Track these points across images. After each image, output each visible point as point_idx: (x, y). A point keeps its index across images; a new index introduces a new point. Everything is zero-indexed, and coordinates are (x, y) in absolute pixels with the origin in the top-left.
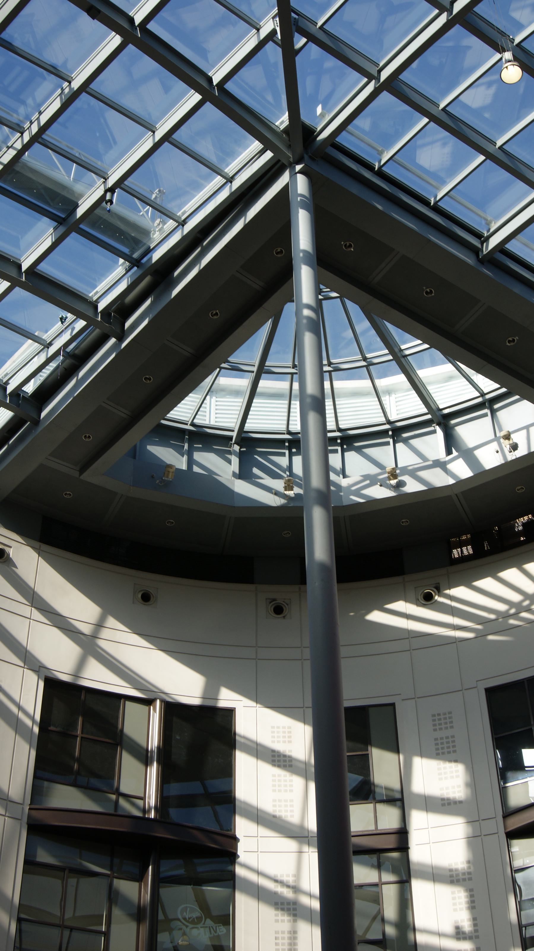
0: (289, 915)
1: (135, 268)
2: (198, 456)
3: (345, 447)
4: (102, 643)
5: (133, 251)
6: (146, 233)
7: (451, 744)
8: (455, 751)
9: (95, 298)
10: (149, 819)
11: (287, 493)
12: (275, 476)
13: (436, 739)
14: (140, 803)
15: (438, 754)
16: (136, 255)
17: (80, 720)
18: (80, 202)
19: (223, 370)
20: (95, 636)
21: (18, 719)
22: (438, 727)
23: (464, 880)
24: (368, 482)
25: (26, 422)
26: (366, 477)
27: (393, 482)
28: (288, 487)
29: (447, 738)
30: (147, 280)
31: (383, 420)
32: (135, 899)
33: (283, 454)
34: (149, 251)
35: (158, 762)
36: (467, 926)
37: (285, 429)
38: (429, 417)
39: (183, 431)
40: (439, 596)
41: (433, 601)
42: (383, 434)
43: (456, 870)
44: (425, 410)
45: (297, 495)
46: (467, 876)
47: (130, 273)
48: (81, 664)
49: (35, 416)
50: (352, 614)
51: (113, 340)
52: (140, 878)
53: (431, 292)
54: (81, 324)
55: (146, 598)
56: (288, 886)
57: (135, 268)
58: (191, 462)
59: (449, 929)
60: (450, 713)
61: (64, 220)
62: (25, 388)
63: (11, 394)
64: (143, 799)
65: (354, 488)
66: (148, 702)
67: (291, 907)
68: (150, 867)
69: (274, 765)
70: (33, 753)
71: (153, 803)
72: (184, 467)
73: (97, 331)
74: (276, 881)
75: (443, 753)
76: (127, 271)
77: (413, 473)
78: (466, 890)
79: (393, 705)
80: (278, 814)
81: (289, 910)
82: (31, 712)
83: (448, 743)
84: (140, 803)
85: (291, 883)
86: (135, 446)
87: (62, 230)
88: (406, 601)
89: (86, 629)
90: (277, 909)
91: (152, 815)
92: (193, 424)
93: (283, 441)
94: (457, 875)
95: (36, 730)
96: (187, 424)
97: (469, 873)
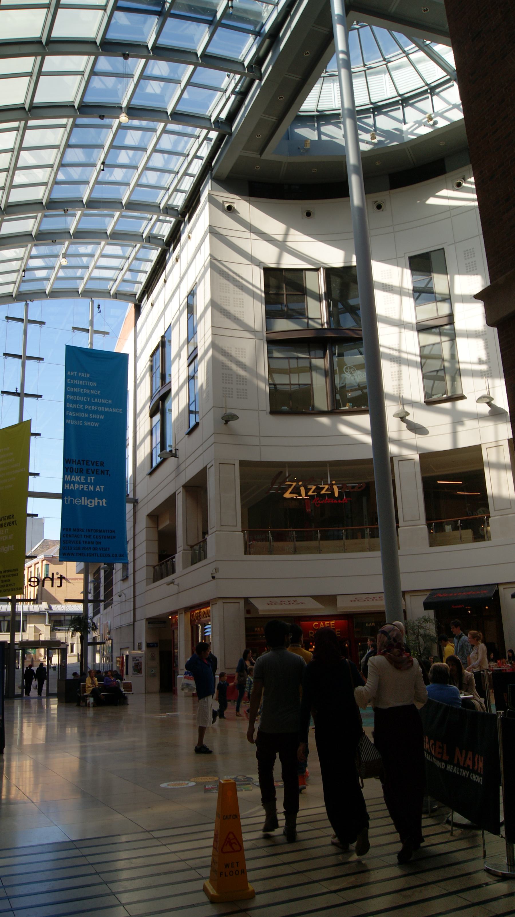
0: (397, 363)
1: (258, 37)
2: (323, 129)
3: (404, 105)
4: (288, 244)
5: (255, 27)
6: (259, 14)
7: (474, 266)
8: (476, 269)
9: (242, 59)
10: (325, 329)
11: (373, 141)
12: (367, 131)
13: (466, 264)
14: (319, 321)
15: (467, 272)
16: (257, 29)
17: (284, 285)
18: (217, 9)
19: (325, 78)
20: (285, 241)
21: (253, 291)
22: (467, 257)
23: (483, 335)
24: (417, 125)
25: (225, 136)
26: (416, 122)
27: (431, 123)
28: (373, 138)
29: (472, 262)
30: (267, 41)
31: (423, 84)
32: (323, 367)
33: (370, 117)
34: (263, 25)
35: (326, 300)
36: (484, 357)
37: (369, 102)
38: (448, 77)
39: (313, 116)
40: (465, 183)
41: (462, 187)
42: (425, 92)
43: (479, 331)
44: (445, 74)
45: (379, 141)
46: (484, 333)
47: (257, 40)
48: (280, 257)
49: (229, 131)
50: (418, 202)
51: (257, 81)
52: (324, 357)
53: (427, 10)
54: (238, 77)
55: (309, 214)
56: (396, 350)
57: (258, 37)
58: (320, 134)
59: (476, 360)
60: (473, 249)
61: (212, 21)
62: (220, 116)
63: (214, 122)
64: (320, 319)
65: (410, 131)
66: (317, 270)
67: (398, 359)
68: (328, 351)
69: (384, 291)
70: (264, 307)
71: (325, 320)
72: (316, 138)
73: (248, 79)
74: (390, 348)
75: (470, 271)
76: (255, 40)
77: (441, 115)
78: (484, 340)
79: (443, 249)
80: (388, 315)
81: (397, 361)
82: (259, 287)
83: (472, 265)
84: (319, 321)
85: (397, 348)
86: (288, 130)
87: (212, 28)
88: (447, 189)
89: (280, 238)
90: (391, 361)
91: (326, 326)
92: (318, 111)
93: (369, 109)
94: (479, 333)
95: (263, 295)
96: (314, 112)
97: (485, 331)
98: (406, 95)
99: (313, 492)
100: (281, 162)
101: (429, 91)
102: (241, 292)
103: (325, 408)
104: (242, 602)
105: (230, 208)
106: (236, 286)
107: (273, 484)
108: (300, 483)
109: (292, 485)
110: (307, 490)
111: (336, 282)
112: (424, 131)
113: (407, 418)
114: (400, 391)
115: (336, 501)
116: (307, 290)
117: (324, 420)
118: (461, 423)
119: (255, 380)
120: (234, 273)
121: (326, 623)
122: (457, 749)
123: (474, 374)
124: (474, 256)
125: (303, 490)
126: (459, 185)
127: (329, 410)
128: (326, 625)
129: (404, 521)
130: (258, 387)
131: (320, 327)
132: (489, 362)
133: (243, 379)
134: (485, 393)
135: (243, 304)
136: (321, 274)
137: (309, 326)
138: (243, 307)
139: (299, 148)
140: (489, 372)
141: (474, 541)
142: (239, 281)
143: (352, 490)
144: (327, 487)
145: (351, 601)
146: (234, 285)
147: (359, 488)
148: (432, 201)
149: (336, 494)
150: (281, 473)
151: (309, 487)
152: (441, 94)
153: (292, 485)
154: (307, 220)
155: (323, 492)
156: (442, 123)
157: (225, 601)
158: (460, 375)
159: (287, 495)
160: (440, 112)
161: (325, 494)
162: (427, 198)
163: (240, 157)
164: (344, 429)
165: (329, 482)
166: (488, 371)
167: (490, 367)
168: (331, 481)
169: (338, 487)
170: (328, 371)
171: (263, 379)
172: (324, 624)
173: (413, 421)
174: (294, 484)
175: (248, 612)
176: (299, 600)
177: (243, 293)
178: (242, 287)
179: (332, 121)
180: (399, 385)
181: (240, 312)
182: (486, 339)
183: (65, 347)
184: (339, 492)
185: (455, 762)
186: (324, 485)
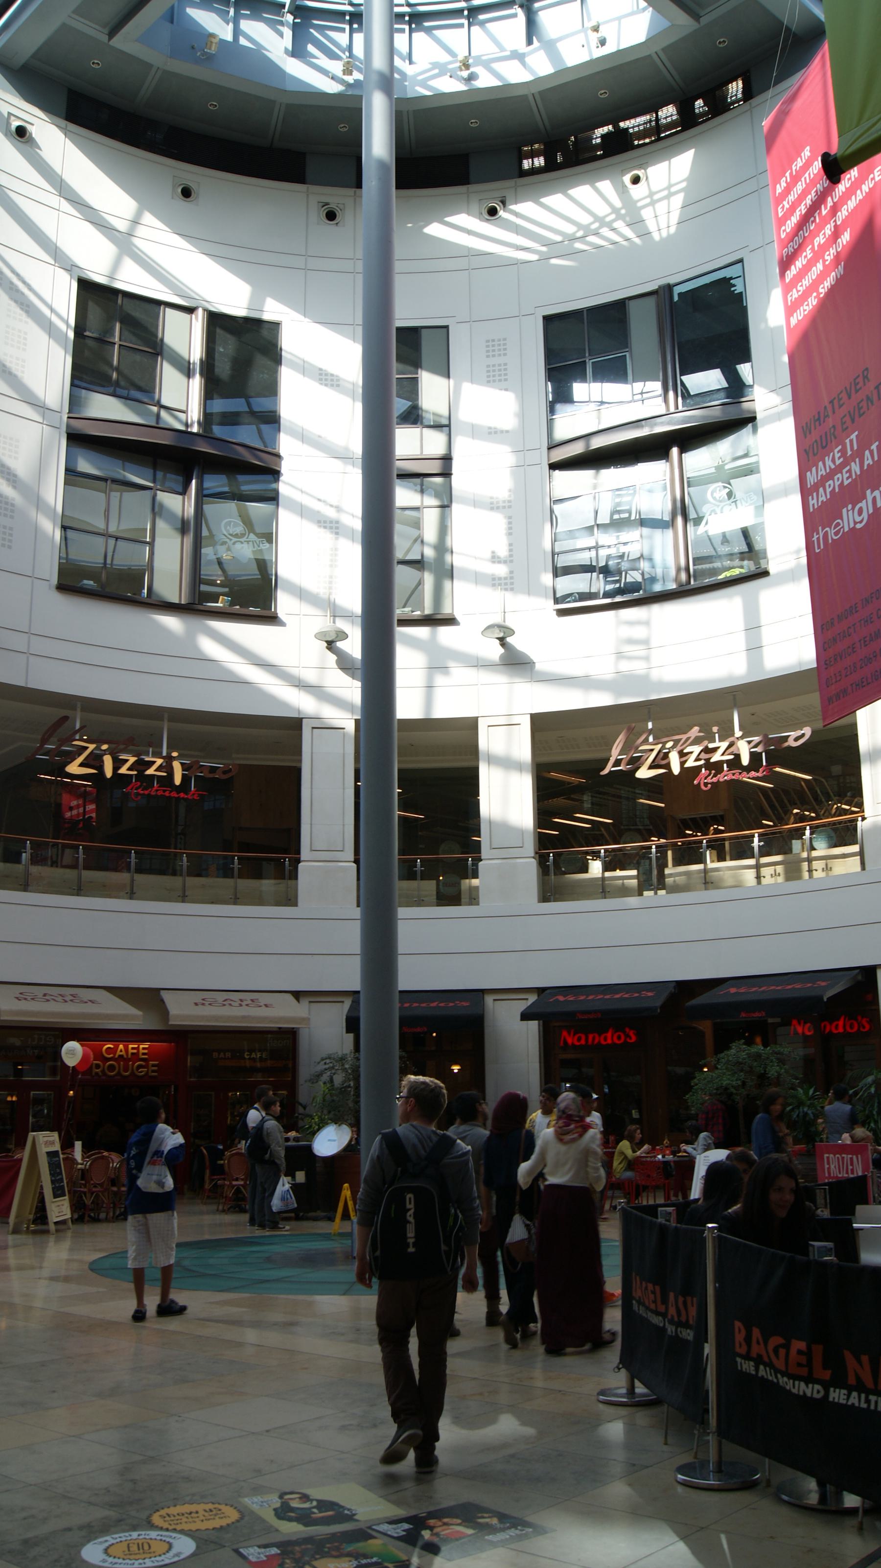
2: (246, 25)
3: (413, 26)
4: (136, 241)
8: (506, 380)
13: (488, 366)
14: (182, 416)
15: (489, 382)
20: (130, 235)
21: (51, 322)
22: (491, 354)
24: (436, 71)
27: (465, 74)
28: (348, 71)
35: (201, 374)
36: (503, 552)
40: (504, 211)
46: (507, 504)
48: (116, 265)
50: (410, 225)
52: (184, 492)
55: (186, 193)
56: (331, 506)
58: (237, 32)
60: (505, 339)
65: (420, 78)
68: (194, 482)
72: (229, 37)
75: (494, 381)
81: (331, 528)
82: (64, 314)
84: (182, 416)
86: (172, 8)
88: (469, 214)
89: (122, 226)
93: (342, 14)
95: (71, 335)
97: (509, 501)
98: (422, 9)
99: (129, 769)
100: (149, 66)
101: (466, 13)
102: (24, 316)
103: (173, 596)
105: (21, 132)
106: (16, 302)
107: (44, 741)
108: (105, 747)
109: (87, 748)
110: (118, 763)
111: (227, 347)
112: (449, 85)
113: (340, 644)
114: (330, 588)
116: (165, 347)
117: (172, 622)
118: (444, 669)
119: (33, 512)
120: (13, 271)
121: (131, 1046)
122: (848, 1355)
123: (478, 578)
124: (505, 355)
126: (493, 212)
127: (183, 602)
128: (131, 1051)
129: (312, 850)
130: (36, 529)
131: (182, 428)
132: (511, 561)
133: (7, 503)
134: (498, 620)
135: (25, 344)
136: (197, 318)
137: (160, 422)
138: (24, 350)
139: (193, 47)
140: (509, 581)
141: (438, 905)
142: (23, 294)
143: (211, 776)
144: (159, 761)
145: (196, 1004)
146: (11, 299)
147: (225, 772)
148: (434, 229)
149: (178, 780)
150: (65, 719)
152: (489, 25)
153: (87, 748)
154: (181, 203)
155: (150, 771)
156: (485, 81)
158: (452, 578)
159: (74, 768)
160: (484, 58)
161: (153, 776)
162: (428, 224)
163: (64, 28)
164: (209, 647)
165: (164, 754)
166: (505, 578)
167: (511, 572)
169: (182, 764)
170: (188, 521)
171: (49, 512)
173: (351, 653)
174: (92, 747)
176: (264, 998)
177: (29, 321)
178: (28, 306)
179: (265, 15)
180: (331, 577)
181: (17, 359)
182: (510, 518)
184: (183, 775)
185: (852, 1380)
186: (153, 756)
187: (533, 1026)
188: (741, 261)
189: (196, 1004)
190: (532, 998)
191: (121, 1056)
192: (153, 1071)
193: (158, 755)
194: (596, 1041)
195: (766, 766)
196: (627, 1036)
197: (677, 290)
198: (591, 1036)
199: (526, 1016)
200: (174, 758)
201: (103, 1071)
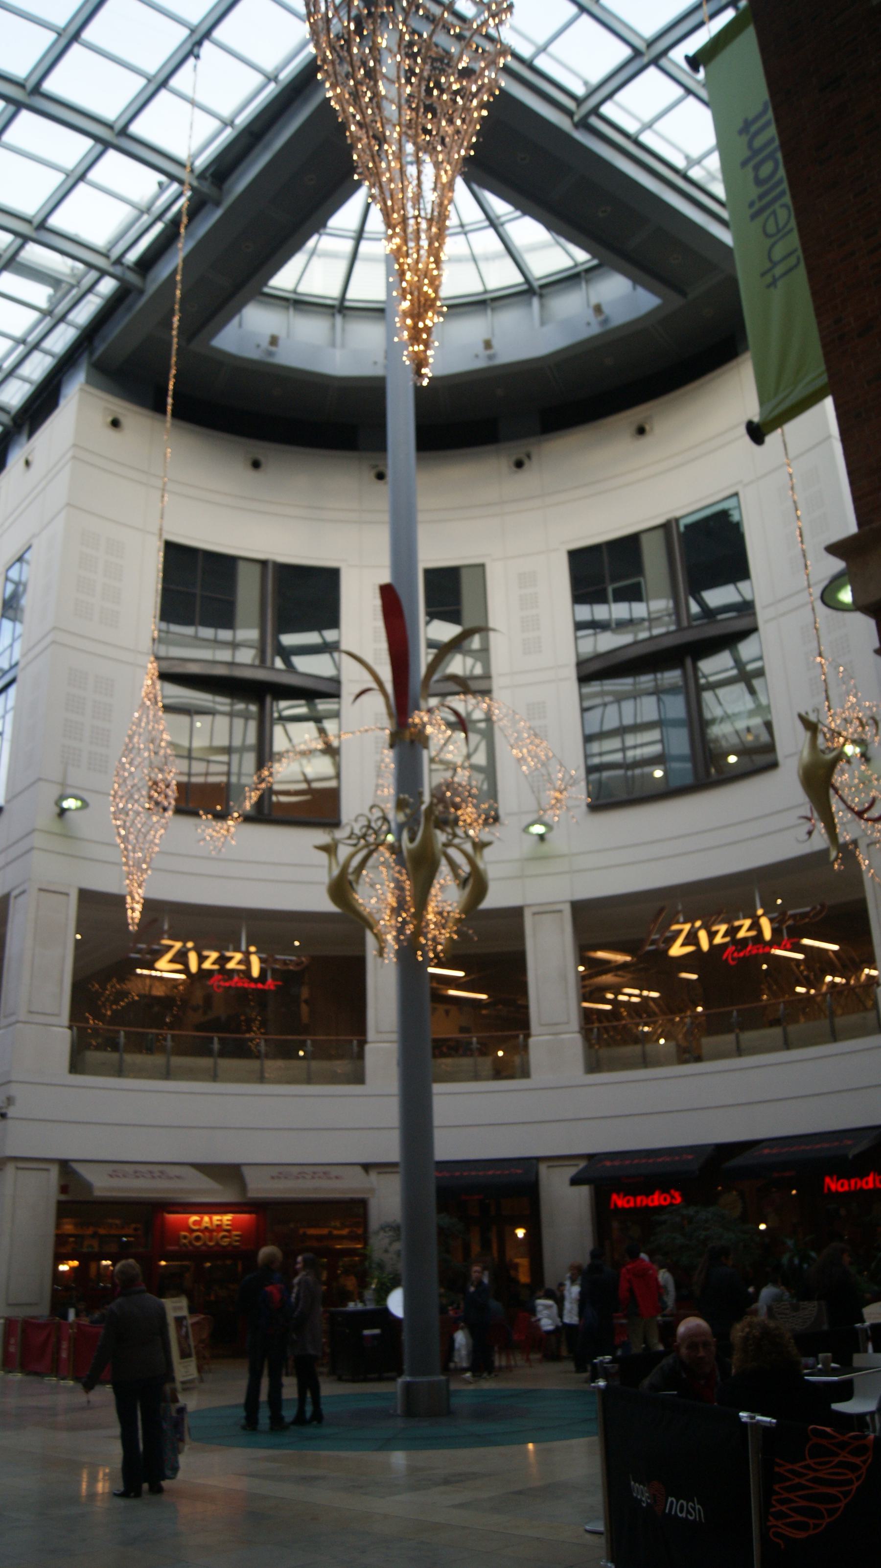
55: (256, 465)
104: (54, 1173)
110: (712, 935)
115: (253, 985)
125: (703, 935)
145: (273, 1178)
151: (715, 928)
157: (21, 1165)
165: (243, 948)
168: (247, 947)
172: (211, 1219)
175: (64, 1189)
176: (335, 1171)
183: (162, 546)
187: (584, 1191)
188: (736, 494)
189: (273, 1178)
190: (582, 1164)
191: (206, 1228)
192: (237, 1241)
193: (237, 949)
194: (858, 1186)
195: (788, 940)
196: (673, 1197)
197: (682, 523)
198: (853, 1181)
199: (575, 1181)
200: (189, 950)
201: (190, 1242)
